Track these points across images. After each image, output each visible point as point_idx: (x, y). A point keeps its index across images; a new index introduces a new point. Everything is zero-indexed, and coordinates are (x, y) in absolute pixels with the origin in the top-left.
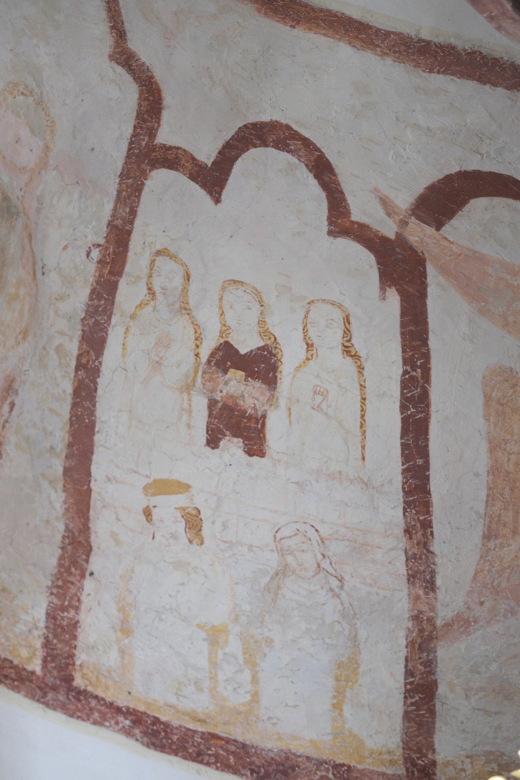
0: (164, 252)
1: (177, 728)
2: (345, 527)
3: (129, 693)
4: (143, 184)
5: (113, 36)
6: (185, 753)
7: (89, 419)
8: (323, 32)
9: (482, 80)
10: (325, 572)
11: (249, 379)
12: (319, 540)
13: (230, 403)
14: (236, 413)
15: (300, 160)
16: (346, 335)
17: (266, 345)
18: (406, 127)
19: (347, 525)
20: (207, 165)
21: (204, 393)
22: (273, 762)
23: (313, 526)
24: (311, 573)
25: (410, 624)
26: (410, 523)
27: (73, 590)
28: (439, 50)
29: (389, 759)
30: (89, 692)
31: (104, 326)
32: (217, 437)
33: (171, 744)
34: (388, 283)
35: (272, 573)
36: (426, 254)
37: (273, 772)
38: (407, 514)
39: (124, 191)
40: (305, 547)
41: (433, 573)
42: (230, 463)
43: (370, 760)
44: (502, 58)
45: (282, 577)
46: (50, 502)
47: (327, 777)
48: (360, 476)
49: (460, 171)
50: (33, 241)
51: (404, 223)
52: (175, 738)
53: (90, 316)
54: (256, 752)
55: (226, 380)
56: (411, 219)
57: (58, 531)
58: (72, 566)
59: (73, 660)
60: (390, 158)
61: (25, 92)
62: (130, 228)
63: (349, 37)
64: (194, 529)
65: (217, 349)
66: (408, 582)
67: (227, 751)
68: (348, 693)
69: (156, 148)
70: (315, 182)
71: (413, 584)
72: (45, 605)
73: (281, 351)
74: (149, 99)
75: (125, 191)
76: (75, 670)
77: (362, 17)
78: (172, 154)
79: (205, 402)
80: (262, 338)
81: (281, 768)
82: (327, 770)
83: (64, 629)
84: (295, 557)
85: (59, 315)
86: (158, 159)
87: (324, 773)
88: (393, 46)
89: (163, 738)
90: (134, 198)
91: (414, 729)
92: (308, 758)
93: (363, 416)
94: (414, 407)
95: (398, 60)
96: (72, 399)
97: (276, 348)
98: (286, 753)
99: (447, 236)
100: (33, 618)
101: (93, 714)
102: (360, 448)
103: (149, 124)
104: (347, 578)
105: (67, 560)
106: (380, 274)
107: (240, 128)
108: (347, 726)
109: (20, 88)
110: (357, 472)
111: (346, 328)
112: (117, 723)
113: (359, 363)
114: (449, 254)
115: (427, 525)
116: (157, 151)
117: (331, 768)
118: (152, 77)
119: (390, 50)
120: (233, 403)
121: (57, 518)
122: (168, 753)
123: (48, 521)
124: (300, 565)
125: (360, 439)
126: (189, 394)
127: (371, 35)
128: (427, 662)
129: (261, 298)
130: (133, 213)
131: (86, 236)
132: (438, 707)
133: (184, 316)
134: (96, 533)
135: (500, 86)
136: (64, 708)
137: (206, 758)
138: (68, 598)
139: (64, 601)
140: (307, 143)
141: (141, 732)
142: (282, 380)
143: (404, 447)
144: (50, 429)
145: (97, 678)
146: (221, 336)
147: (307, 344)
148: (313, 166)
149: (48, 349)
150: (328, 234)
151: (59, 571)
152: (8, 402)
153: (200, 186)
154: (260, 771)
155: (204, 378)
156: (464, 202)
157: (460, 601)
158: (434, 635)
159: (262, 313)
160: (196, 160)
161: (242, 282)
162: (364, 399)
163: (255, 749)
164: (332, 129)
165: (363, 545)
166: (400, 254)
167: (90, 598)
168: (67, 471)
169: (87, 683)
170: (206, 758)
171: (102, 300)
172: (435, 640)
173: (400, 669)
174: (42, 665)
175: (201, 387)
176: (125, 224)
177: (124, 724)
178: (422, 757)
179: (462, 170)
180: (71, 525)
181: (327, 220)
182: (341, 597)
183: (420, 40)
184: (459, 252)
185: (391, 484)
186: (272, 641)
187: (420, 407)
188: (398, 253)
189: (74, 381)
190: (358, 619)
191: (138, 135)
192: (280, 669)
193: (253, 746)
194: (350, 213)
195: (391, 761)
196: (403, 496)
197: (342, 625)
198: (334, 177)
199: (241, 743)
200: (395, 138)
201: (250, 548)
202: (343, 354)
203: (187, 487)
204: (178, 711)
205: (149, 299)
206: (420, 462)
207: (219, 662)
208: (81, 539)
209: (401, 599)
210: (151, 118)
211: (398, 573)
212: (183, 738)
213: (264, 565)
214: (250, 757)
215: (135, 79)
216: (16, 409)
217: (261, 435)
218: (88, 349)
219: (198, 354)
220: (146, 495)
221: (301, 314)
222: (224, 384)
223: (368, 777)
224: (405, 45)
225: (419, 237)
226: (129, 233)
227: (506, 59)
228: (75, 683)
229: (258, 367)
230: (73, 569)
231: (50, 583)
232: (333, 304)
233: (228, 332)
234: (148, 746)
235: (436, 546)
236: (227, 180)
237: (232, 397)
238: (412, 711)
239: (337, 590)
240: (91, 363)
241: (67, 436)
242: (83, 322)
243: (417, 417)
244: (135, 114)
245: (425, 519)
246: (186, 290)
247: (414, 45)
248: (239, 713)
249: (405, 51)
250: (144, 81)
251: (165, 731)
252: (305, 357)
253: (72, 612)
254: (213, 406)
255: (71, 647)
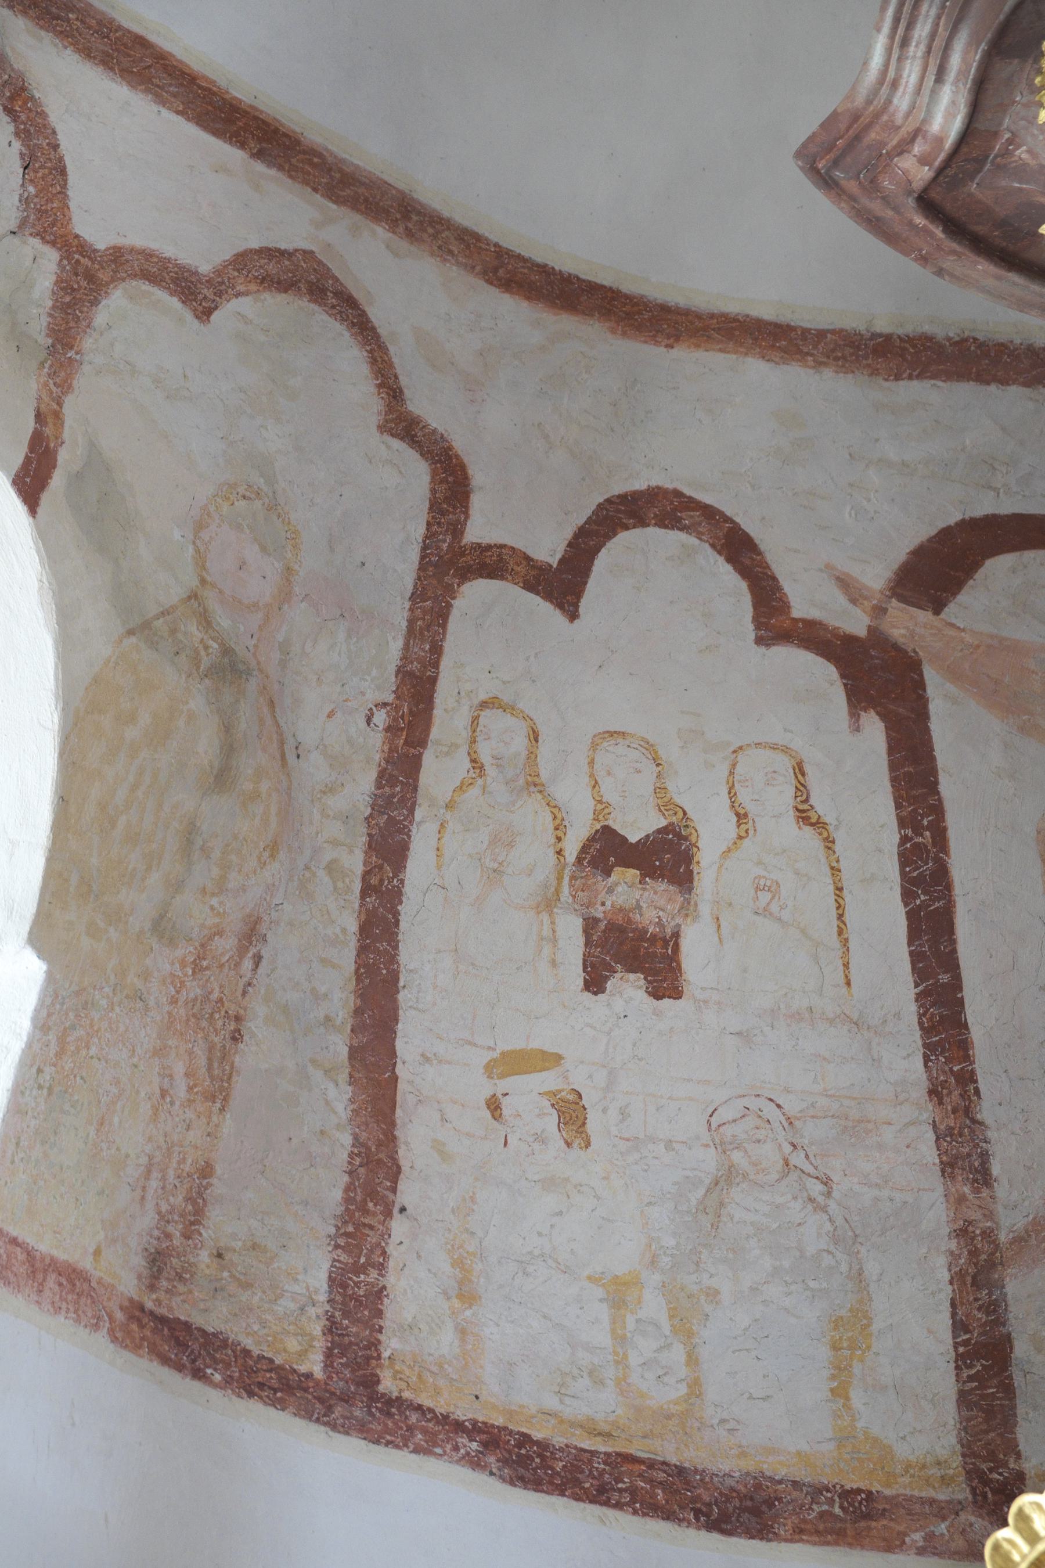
0: (493, 703)
1: (561, 1450)
2: (826, 1096)
3: (477, 1397)
4: (449, 606)
5: (382, 398)
6: (577, 1490)
7: (387, 969)
8: (718, 347)
9: (983, 378)
10: (799, 1172)
11: (647, 879)
12: (784, 1122)
13: (619, 920)
14: (631, 935)
15: (700, 539)
16: (799, 794)
17: (671, 824)
18: (867, 466)
19: (829, 1093)
20: (551, 566)
21: (575, 910)
22: (734, 1494)
23: (771, 1100)
24: (775, 1176)
25: (953, 1245)
26: (937, 1078)
27: (373, 1238)
28: (907, 345)
29: (939, 1475)
30: (406, 1400)
31: (403, 825)
32: (601, 975)
33: (551, 1476)
34: (863, 704)
35: (707, 1181)
36: (921, 653)
37: (734, 1511)
38: (930, 1064)
39: (418, 619)
40: (761, 1134)
41: (985, 1156)
42: (625, 1014)
43: (906, 1480)
44: (1012, 342)
45: (726, 1187)
46: (327, 1103)
47: (830, 1514)
48: (845, 1011)
49: (963, 521)
50: (277, 709)
51: (879, 611)
52: (559, 1466)
53: (379, 812)
54: (702, 1480)
55: (609, 885)
56: (890, 602)
57: (342, 1145)
58: (368, 1199)
59: (377, 1350)
60: (847, 515)
61: (248, 494)
62: (433, 672)
63: (760, 348)
64: (573, 1124)
65: (592, 839)
66: (943, 1175)
67: (651, 1481)
68: (857, 1369)
69: (465, 551)
70: (729, 568)
71: (952, 1177)
72: (326, 1266)
73: (696, 831)
74: (447, 480)
75: (421, 619)
76: (381, 1366)
77: (777, 316)
78: (491, 556)
79: (579, 922)
80: (664, 814)
81: (749, 1503)
82: (831, 1502)
83: (361, 1302)
84: (746, 1151)
85: (329, 816)
86: (471, 566)
87: (825, 1507)
88: (833, 351)
89: (537, 1468)
90: (437, 628)
91: (980, 1420)
92: (795, 1484)
93: (840, 917)
94: (925, 893)
95: (844, 370)
96: (359, 941)
97: (687, 826)
98: (755, 1478)
99: (954, 621)
100: (308, 1289)
101: (413, 1435)
102: (842, 968)
103: (451, 516)
104: (835, 1178)
105: (359, 1190)
106: (847, 695)
107: (599, 505)
108: (860, 1425)
109: (239, 490)
110: (839, 1006)
111: (799, 782)
112: (456, 1448)
113: (825, 834)
114: (959, 648)
115: (967, 1079)
116: (468, 554)
117: (836, 1498)
118: (450, 448)
119: (828, 357)
120: (624, 919)
121: (338, 1127)
122: (547, 1493)
123: (322, 1132)
124: (755, 1165)
125: (840, 953)
126: (551, 914)
127: (796, 339)
128: (990, 1305)
129: (656, 752)
130: (437, 650)
131: (363, 694)
132: (1018, 1380)
133: (533, 795)
134: (407, 1143)
135: (1014, 383)
136: (363, 1430)
137: (616, 1496)
138: (365, 1251)
139: (359, 1258)
140: (709, 512)
141: (498, 1461)
142: (701, 875)
143: (916, 957)
144: (323, 989)
145: (420, 1376)
146: (596, 820)
147: (737, 815)
148: (722, 545)
149: (313, 868)
150: (756, 643)
151: (347, 1209)
152: (250, 954)
153: (542, 597)
154: (712, 1510)
155: (573, 886)
156: (976, 566)
157: (1037, 1197)
158: (997, 1258)
159: (659, 776)
160: (532, 560)
161: (623, 733)
162: (841, 889)
163: (701, 1475)
164: (748, 485)
165: (860, 1121)
166: (877, 658)
167: (402, 1248)
168: (354, 1053)
169: (404, 1385)
170: (616, 1496)
171: (397, 786)
172: (1000, 1268)
173: (943, 1321)
174: (325, 1362)
175: (570, 900)
176: (424, 667)
177: (468, 1449)
178: (998, 1468)
179: (967, 517)
180: (364, 1136)
181: (752, 622)
182: (829, 1209)
183: (874, 336)
184: (976, 642)
185: (899, 1019)
186: (717, 1292)
187: (935, 891)
188: (872, 657)
189: (360, 913)
190: (861, 1244)
191: (434, 534)
192: (735, 1338)
193: (696, 1471)
194: (789, 607)
195: (942, 1477)
196: (921, 1035)
197: (834, 1257)
198: (758, 558)
199: (676, 1466)
200: (851, 485)
201: (669, 1145)
202: (798, 822)
203: (558, 1058)
204: (562, 1421)
205: (474, 775)
206: (944, 978)
207: (629, 1335)
208: (382, 1156)
209: (933, 1205)
210: (453, 508)
211: (925, 1162)
212: (572, 1465)
213: (695, 1169)
214: (693, 1489)
215: (422, 455)
216: (264, 963)
217: (674, 964)
218: (380, 862)
219: (561, 850)
220: (490, 1077)
221: (724, 769)
222: (607, 893)
223: (904, 1507)
224: (850, 347)
225: (908, 628)
226: (434, 680)
227: (1018, 341)
228: (381, 1388)
229: (661, 860)
230: (371, 1205)
231: (332, 1231)
232: (774, 747)
233: (606, 811)
234: (512, 1483)
235: (986, 1112)
236: (585, 583)
237: (621, 910)
238: (972, 1389)
239: (821, 1199)
240: (386, 882)
241: (352, 997)
242: (369, 822)
243: (932, 908)
244: (427, 504)
245: (962, 1069)
246: (533, 756)
247: (865, 345)
248: (669, 1417)
249: (851, 355)
250: (437, 455)
251: (540, 1455)
252: (735, 836)
253: (374, 1274)
254: (592, 929)
255: (373, 1330)
